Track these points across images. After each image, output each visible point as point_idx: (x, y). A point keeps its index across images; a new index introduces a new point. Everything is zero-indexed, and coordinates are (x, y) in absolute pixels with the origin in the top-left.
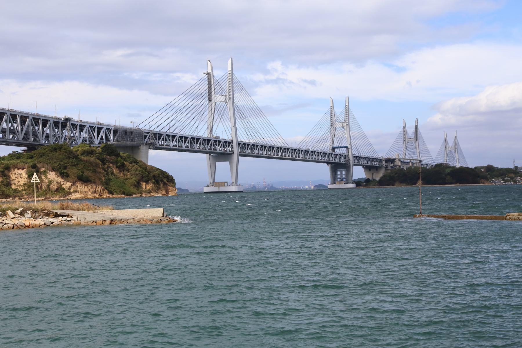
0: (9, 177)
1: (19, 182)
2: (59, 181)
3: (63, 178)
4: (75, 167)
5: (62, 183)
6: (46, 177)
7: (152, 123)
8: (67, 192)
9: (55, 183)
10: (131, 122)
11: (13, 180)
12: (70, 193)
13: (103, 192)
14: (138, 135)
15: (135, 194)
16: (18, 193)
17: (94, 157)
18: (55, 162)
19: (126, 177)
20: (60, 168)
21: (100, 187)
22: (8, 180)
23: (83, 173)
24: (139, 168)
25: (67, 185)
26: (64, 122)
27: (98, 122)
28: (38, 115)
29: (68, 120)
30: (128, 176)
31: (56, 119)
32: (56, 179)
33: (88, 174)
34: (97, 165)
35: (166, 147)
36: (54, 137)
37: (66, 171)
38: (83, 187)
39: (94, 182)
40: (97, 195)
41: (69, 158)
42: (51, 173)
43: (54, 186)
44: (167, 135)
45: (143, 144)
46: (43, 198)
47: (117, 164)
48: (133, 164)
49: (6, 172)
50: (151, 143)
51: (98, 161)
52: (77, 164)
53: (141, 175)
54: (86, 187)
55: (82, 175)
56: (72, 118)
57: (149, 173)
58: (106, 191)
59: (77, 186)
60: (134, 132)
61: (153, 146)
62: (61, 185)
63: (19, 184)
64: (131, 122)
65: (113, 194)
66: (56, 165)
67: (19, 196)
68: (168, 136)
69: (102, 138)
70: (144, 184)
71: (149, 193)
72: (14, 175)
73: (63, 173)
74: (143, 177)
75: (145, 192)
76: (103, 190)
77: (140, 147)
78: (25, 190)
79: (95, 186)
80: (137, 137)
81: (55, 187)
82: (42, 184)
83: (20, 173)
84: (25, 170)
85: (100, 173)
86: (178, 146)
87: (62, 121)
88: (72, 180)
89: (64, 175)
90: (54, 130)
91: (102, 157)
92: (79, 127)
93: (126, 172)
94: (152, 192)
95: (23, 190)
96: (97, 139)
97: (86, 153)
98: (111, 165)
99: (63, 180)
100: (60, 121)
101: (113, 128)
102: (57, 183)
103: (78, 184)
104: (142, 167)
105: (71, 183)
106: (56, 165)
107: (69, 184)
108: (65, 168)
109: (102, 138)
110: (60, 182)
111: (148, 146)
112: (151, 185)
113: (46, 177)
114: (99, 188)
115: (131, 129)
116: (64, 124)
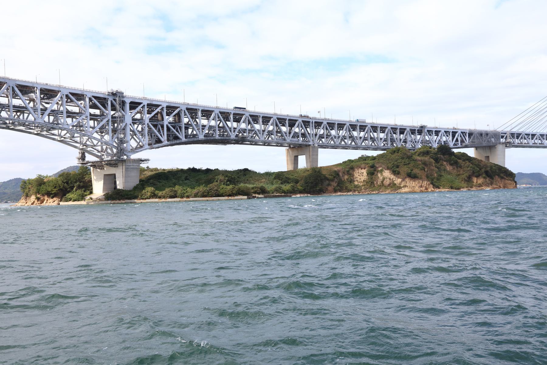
0: (353, 176)
1: (360, 179)
2: (391, 178)
3: (395, 175)
4: (405, 166)
5: (394, 179)
6: (382, 175)
7: (513, 126)
8: (398, 187)
9: (387, 179)
10: (488, 125)
11: (356, 177)
12: (400, 188)
13: (429, 187)
14: (495, 136)
15: (463, 188)
16: (358, 188)
17: (428, 157)
18: (390, 162)
19: (458, 173)
20: (393, 167)
21: (426, 182)
22: (352, 178)
23: (412, 170)
24: (471, 165)
25: (398, 181)
26: (420, 129)
27: (454, 128)
28: (396, 125)
29: (422, 127)
30: (461, 172)
31: (413, 127)
32: (389, 176)
33: (416, 171)
34: (430, 164)
35: (525, 145)
36: (411, 142)
37: (397, 169)
38: (412, 182)
39: (421, 179)
40: (423, 189)
41: (403, 158)
42: (386, 171)
43: (387, 182)
44: (526, 134)
45: (500, 143)
46: (377, 192)
47: (449, 162)
48: (466, 161)
49: (351, 171)
50: (508, 142)
51: (432, 160)
52: (409, 164)
53: (472, 171)
54: (414, 182)
55: (411, 173)
56: (427, 126)
57: (480, 169)
58: (431, 186)
59: (407, 182)
60: (490, 134)
61: (508, 145)
62: (393, 181)
63: (360, 181)
64: (319, 112)
65: (439, 188)
66: (390, 165)
67: (358, 191)
68: (528, 135)
69: (457, 140)
70: (475, 178)
71: (479, 187)
72: (357, 173)
73: (395, 171)
74: (474, 172)
75: (475, 186)
76: (429, 185)
77: (496, 146)
78: (364, 185)
79: (421, 182)
80: (493, 137)
81: (388, 183)
82: (377, 181)
83: (362, 172)
84: (366, 169)
85: (433, 170)
86: (538, 144)
87: (418, 129)
88: (402, 177)
89: (396, 173)
90: (411, 136)
91: (436, 157)
92: (337, 125)
93: (459, 169)
94: (482, 186)
95: (362, 186)
96: (452, 141)
97: (422, 154)
98: (445, 163)
99: (395, 177)
100: (417, 129)
101: (468, 132)
102: (390, 179)
103: (407, 180)
104: (474, 164)
105: (401, 180)
106: (390, 165)
107: (399, 180)
108: (398, 167)
109: (457, 140)
110: (393, 179)
111: (504, 145)
112: (482, 180)
113: (382, 175)
114: (425, 183)
115: (486, 131)
116: (420, 131)
